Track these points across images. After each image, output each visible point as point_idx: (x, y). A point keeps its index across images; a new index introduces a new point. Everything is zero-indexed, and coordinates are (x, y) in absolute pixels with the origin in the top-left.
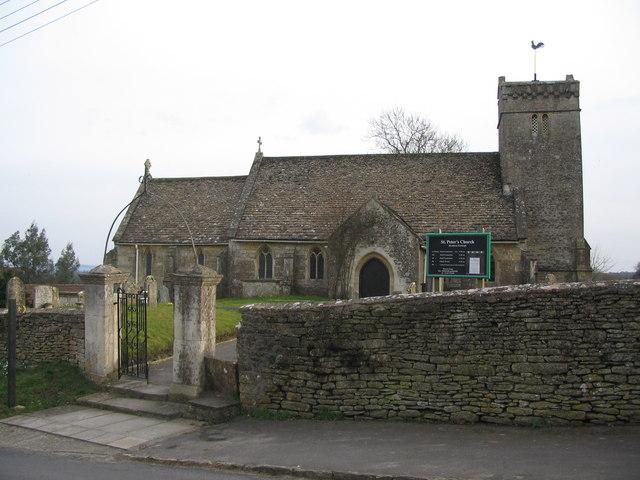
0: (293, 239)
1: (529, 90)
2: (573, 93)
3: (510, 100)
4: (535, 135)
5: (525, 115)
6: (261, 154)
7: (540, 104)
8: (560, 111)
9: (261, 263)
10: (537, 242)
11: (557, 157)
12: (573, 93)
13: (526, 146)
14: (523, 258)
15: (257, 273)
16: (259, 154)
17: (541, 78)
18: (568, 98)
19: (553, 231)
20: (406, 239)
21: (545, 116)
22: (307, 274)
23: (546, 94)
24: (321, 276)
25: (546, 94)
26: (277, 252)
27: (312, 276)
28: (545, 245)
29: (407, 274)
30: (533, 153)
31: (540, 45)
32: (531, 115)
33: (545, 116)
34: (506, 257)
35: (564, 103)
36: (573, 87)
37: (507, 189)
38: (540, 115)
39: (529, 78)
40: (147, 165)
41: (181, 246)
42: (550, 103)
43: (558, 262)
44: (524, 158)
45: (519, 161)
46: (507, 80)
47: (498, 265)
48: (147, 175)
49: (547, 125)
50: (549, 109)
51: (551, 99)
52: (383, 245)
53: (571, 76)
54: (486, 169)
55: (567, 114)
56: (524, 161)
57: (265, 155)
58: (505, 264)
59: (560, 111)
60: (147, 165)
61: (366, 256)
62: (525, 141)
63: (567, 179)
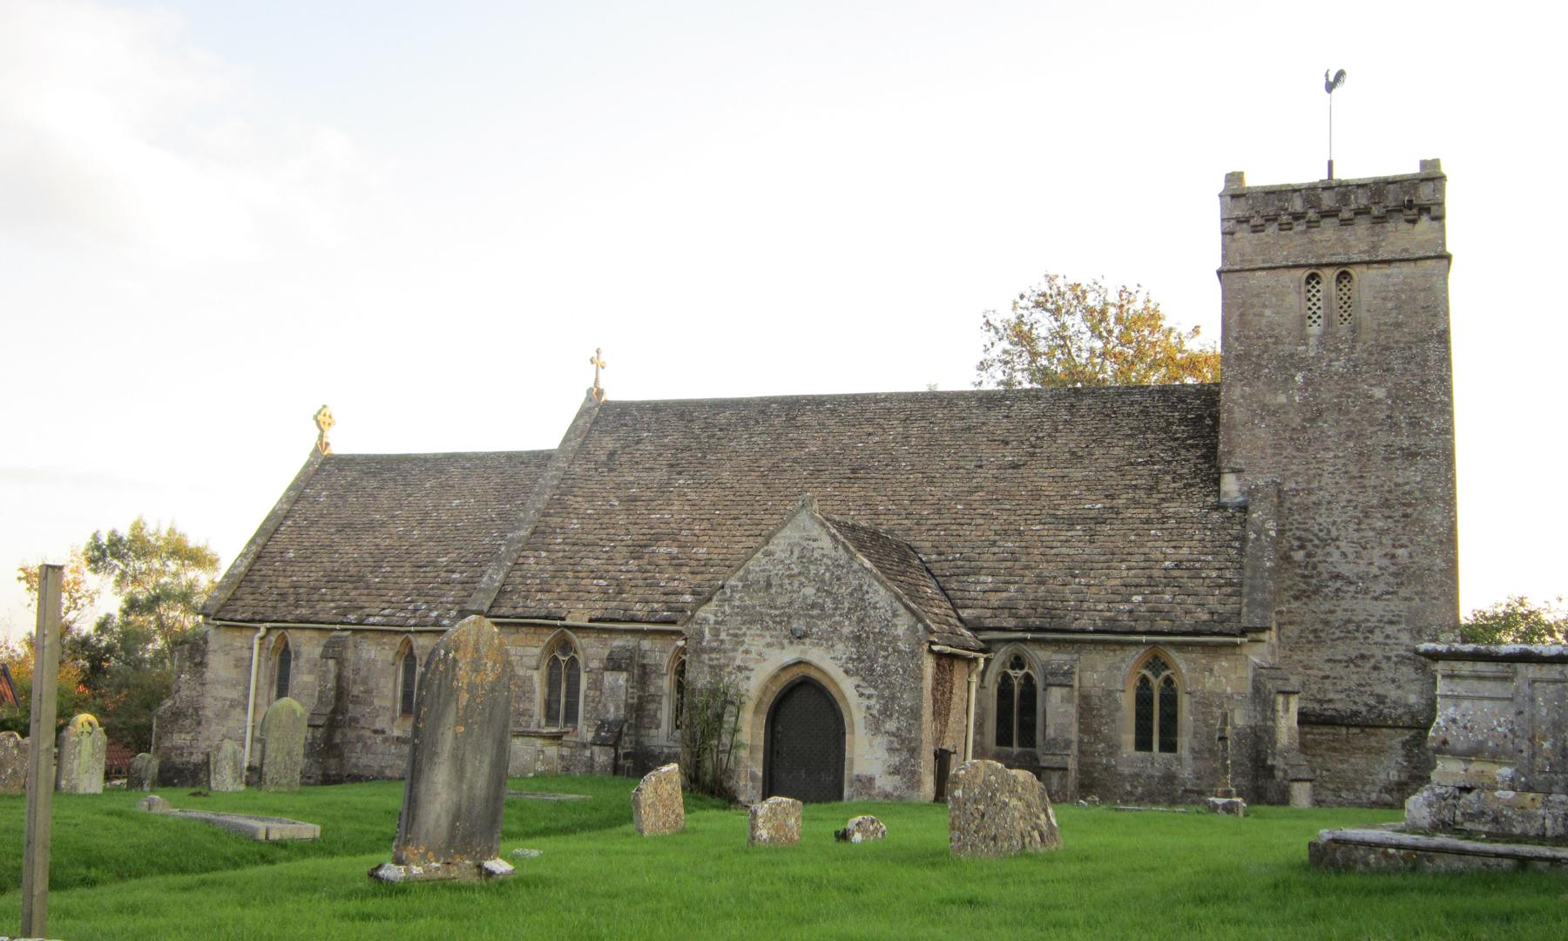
0: (633, 620)
1: (1297, 205)
2: (1424, 209)
3: (1244, 233)
4: (1315, 330)
5: (1286, 276)
6: (600, 393)
7: (1328, 240)
8: (1389, 262)
9: (552, 684)
10: (1319, 641)
11: (1379, 393)
12: (1424, 209)
13: (1291, 363)
14: (1257, 689)
15: (538, 708)
16: (595, 393)
17: (1341, 174)
18: (1413, 222)
19: (1365, 609)
20: (888, 624)
21: (1344, 276)
22: (1128, 738)
23: (1346, 214)
24: (1169, 745)
25: (1285, 218)
26: (591, 651)
27: (1143, 743)
28: (1342, 650)
29: (891, 725)
30: (1308, 382)
31: (1340, 75)
32: (1303, 274)
33: (1344, 276)
34: (1209, 683)
35: (1401, 236)
36: (1425, 193)
37: (1231, 486)
38: (1329, 275)
39: (1317, 175)
40: (322, 420)
41: (361, 629)
42: (1357, 241)
43: (1381, 699)
44: (1282, 399)
45: (1264, 406)
46: (1252, 181)
47: (1185, 705)
48: (322, 443)
49: (1347, 303)
50: (1356, 258)
51: (1362, 226)
52: (826, 640)
53: (1435, 163)
54: (1180, 431)
55: (1407, 269)
56: (1282, 406)
57: (614, 394)
58: (1204, 704)
59: (1389, 262)
60: (322, 420)
61: (775, 677)
62: (1286, 349)
63: (1410, 455)
